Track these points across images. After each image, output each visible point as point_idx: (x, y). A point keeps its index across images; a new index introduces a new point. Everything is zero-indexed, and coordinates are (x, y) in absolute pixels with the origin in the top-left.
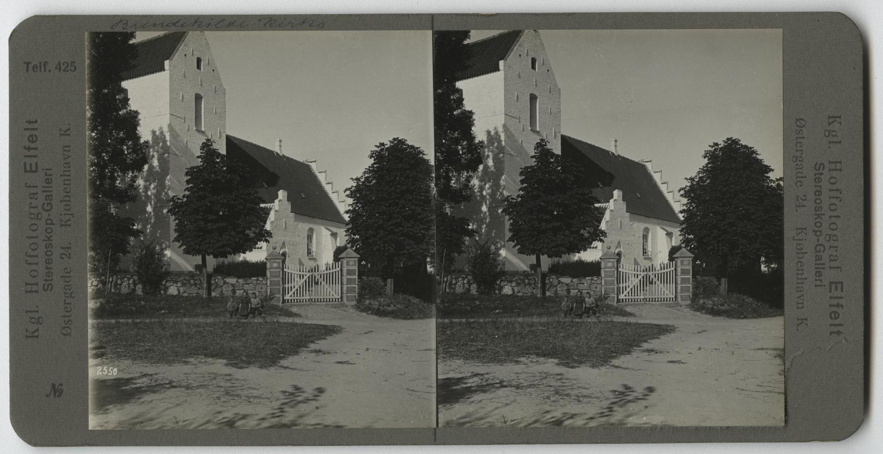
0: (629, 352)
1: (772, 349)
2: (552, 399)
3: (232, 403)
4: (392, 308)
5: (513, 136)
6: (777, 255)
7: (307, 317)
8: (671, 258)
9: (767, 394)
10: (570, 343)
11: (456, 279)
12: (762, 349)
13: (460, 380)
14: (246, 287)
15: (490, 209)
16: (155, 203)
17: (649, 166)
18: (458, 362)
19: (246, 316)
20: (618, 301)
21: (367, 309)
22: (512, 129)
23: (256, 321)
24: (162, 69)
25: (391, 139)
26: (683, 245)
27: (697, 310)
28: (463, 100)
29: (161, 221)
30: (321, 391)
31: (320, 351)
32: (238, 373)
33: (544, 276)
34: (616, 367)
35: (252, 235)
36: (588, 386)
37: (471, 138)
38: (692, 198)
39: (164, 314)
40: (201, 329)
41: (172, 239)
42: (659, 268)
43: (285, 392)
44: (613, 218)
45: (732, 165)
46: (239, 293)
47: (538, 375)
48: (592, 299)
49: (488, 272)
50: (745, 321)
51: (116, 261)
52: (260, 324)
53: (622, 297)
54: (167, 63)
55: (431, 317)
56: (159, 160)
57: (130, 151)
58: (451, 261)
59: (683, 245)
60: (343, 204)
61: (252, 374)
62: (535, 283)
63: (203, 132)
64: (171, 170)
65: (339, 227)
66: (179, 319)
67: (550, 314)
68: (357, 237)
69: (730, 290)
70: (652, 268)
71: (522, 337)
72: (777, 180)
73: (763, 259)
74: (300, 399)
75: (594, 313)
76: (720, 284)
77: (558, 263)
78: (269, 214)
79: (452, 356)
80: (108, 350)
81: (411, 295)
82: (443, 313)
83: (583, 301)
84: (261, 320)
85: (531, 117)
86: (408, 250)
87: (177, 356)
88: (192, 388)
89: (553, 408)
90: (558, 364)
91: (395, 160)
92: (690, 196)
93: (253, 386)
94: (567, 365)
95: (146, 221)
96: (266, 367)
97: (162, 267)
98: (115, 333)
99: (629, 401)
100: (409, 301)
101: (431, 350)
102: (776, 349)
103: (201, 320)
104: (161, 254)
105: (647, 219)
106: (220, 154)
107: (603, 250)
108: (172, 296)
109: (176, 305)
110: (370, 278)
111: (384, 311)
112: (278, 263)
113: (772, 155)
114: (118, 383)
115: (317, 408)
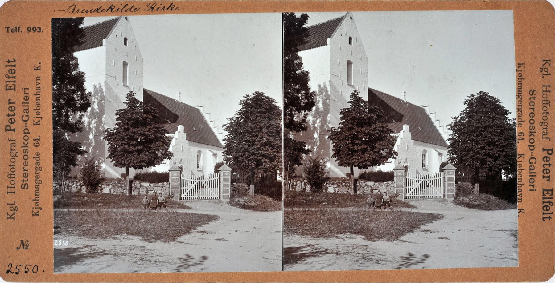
0: (412, 232)
1: (509, 231)
2: (360, 262)
3: (366, 264)
4: (253, 204)
5: (336, 88)
6: (512, 167)
7: (196, 209)
8: (441, 170)
9: (505, 260)
10: (372, 225)
11: (296, 182)
12: (502, 230)
13: (298, 249)
14: (155, 189)
15: (95, 136)
16: (320, 132)
17: (427, 109)
18: (297, 237)
19: (155, 208)
20: (181, 199)
21: (460, 204)
22: (110, 85)
23: (161, 211)
24: (101, 45)
25: (254, 92)
26: (225, 162)
27: (458, 204)
28: (302, 64)
29: (99, 145)
30: (205, 258)
31: (428, 231)
32: (149, 246)
33: (356, 181)
34: (181, 243)
35: (160, 155)
36: (385, 254)
37: (307, 89)
38: (231, 131)
39: (100, 206)
40: (124, 216)
41: (106, 156)
42: (433, 176)
43: (181, 259)
44: (177, 144)
45: (483, 109)
46: (151, 193)
47: (351, 246)
48: (163, 197)
49: (317, 178)
50: (490, 212)
51: (69, 171)
52: (165, 213)
53: (183, 196)
54: (104, 41)
55: (280, 210)
56: (323, 104)
57: (79, 98)
58: (293, 170)
59: (225, 162)
60: (222, 135)
61: (159, 246)
62: (125, 186)
63: (128, 87)
64: (106, 111)
65: (218, 150)
66: (334, 209)
67: (135, 207)
68: (455, 156)
69: (481, 191)
70: (428, 176)
71: (340, 221)
72: (514, 119)
73: (503, 171)
74: (191, 263)
75: (389, 206)
76: (474, 188)
77: (365, 172)
78: (171, 141)
79: (293, 232)
80: (62, 229)
81: (266, 195)
82: (288, 204)
83: (381, 198)
84: (389, 210)
85: (348, 76)
86: (489, 165)
87: (108, 234)
88: (118, 255)
89: (139, 269)
90: (364, 239)
91: (257, 105)
92: (230, 130)
93: (381, 253)
94: (370, 240)
95: (314, 144)
96: (391, 241)
97: (99, 175)
98: (67, 218)
99: (412, 264)
100: (490, 198)
101: (279, 232)
102: (511, 231)
103: (125, 210)
104: (99, 166)
105: (200, 145)
106: (139, 101)
107: (395, 164)
108: (331, 193)
109: (109, 200)
110: (464, 183)
111: (248, 206)
112: (402, 172)
113: (509, 102)
114: (68, 251)
115: (202, 269)
